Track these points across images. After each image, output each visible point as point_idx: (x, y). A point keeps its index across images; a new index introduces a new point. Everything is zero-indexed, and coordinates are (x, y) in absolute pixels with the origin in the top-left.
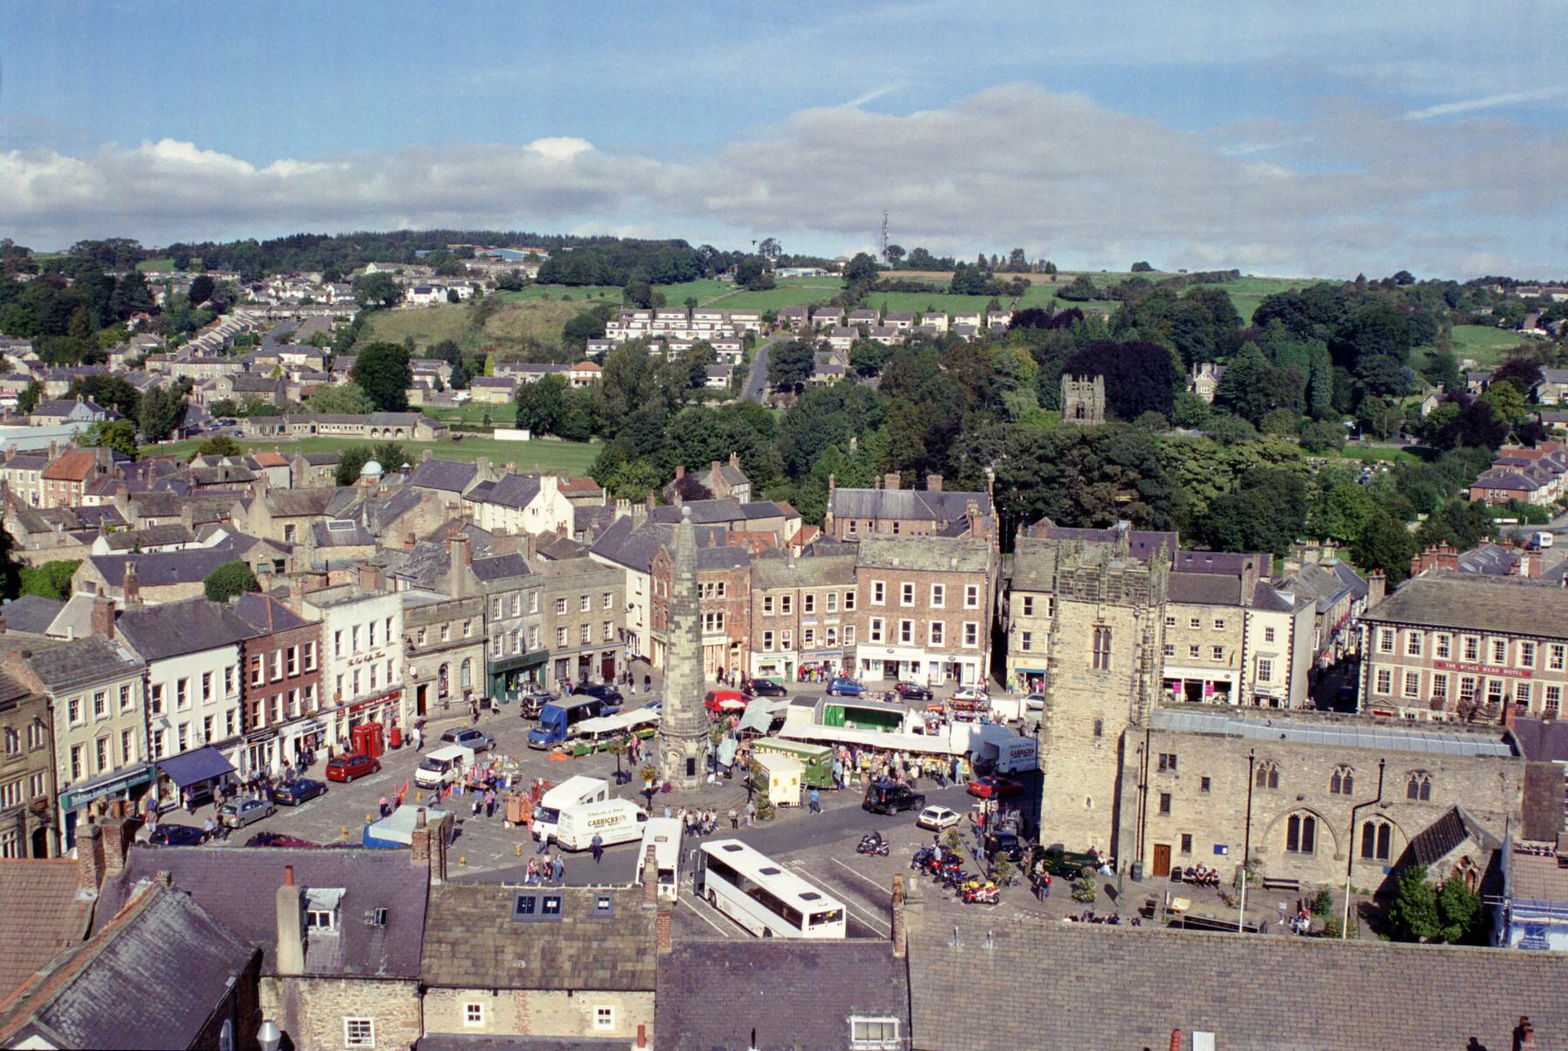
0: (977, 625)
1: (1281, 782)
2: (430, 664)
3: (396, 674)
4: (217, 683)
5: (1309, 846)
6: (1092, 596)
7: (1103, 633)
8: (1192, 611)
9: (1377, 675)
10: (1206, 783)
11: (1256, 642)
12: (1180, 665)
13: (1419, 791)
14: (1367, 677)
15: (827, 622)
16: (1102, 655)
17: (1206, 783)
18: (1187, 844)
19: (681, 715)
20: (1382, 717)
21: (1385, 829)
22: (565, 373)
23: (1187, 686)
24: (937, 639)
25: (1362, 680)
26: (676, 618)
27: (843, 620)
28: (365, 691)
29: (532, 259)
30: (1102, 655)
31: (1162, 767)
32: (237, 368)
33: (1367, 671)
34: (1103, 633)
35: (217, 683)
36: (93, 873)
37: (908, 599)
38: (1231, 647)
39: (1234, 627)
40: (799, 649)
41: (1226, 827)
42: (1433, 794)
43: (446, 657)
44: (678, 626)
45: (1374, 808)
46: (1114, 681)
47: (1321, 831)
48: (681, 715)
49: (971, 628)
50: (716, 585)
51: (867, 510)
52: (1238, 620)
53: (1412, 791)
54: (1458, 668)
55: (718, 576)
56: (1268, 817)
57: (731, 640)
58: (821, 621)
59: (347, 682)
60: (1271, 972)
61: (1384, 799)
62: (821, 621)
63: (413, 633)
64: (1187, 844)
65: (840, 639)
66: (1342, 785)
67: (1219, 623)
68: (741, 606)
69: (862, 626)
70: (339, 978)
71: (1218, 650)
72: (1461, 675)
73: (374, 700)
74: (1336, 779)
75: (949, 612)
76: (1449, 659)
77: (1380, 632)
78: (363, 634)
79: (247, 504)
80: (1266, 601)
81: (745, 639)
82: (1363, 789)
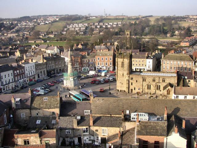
1: (146, 81)
2: (40, 71)
3: (35, 72)
4: (10, 75)
5: (150, 89)
8: (139, 60)
10: (137, 81)
13: (164, 81)
17: (137, 81)
18: (135, 89)
20: (162, 72)
21: (160, 86)
22: (33, 32)
23: (160, 71)
24: (106, 65)
28: (31, 75)
29: (57, 18)
31: (131, 79)
32: (17, 34)
35: (10, 75)
36: (128, 133)
37: (106, 60)
40: (88, 67)
41: (140, 86)
42: (166, 81)
43: (41, 70)
45: (158, 83)
46: (125, 69)
47: (152, 86)
51: (99, 49)
53: (163, 81)
56: (145, 85)
59: (28, 74)
60: (136, 103)
61: (160, 82)
63: (36, 67)
64: (135, 89)
66: (154, 81)
70: (20, 109)
73: (32, 76)
74: (153, 80)
75: (108, 61)
78: (30, 68)
79: (17, 52)
80: (148, 58)
82: (157, 81)
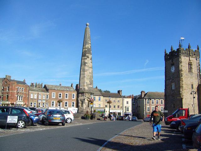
0: (75, 102)
6: (189, 55)
7: (190, 64)
9: (147, 108)
11: (125, 104)
12: (112, 109)
14: (145, 109)
15: (43, 101)
16: (190, 69)
19: (90, 86)
25: (145, 109)
26: (87, 55)
27: (46, 101)
30: (190, 69)
33: (145, 108)
34: (190, 64)
38: (121, 105)
39: (121, 102)
44: (88, 57)
46: (194, 75)
48: (90, 86)
49: (73, 103)
50: (22, 88)
52: (122, 100)
54: (160, 105)
55: (22, 86)
57: (24, 103)
58: (42, 101)
62: (42, 101)
65: (45, 106)
67: (118, 101)
68: (26, 95)
69: (50, 102)
71: (118, 106)
72: (161, 107)
76: (159, 104)
77: (147, 100)
81: (27, 103)
